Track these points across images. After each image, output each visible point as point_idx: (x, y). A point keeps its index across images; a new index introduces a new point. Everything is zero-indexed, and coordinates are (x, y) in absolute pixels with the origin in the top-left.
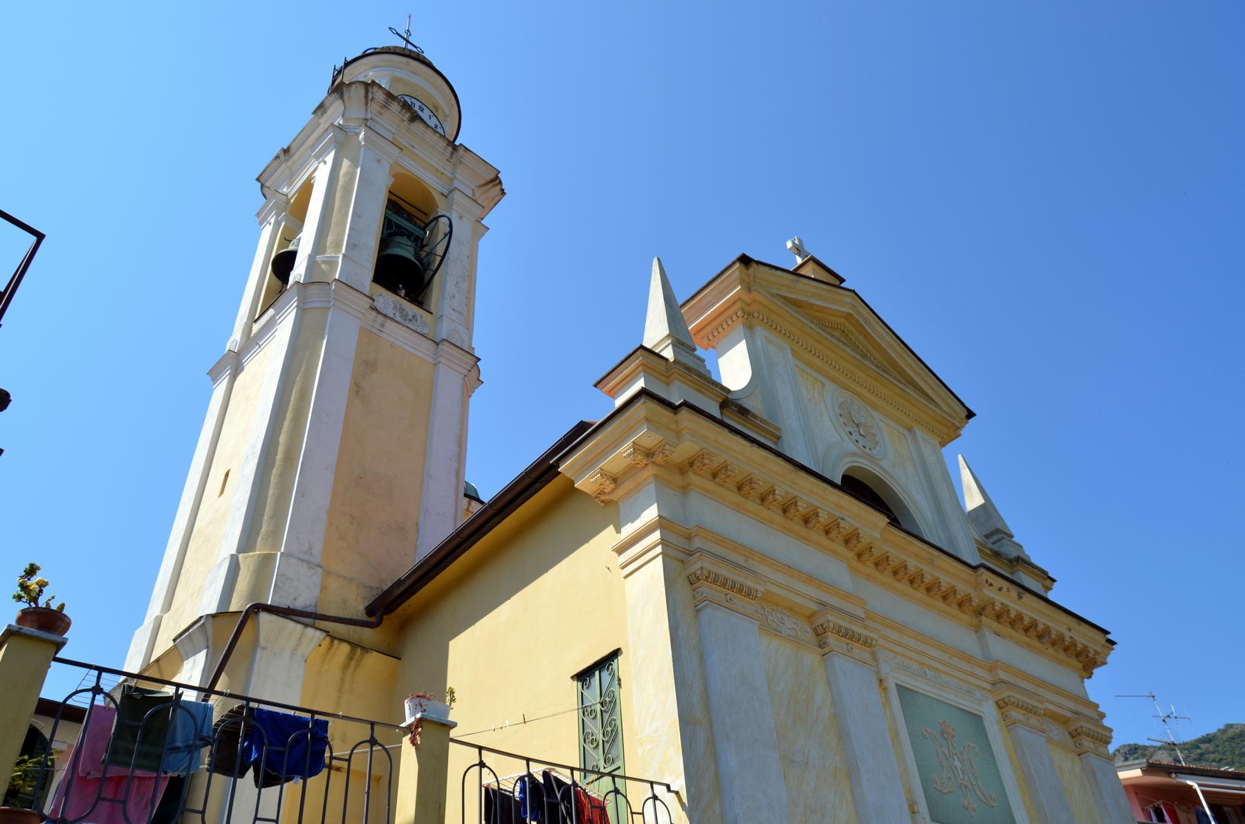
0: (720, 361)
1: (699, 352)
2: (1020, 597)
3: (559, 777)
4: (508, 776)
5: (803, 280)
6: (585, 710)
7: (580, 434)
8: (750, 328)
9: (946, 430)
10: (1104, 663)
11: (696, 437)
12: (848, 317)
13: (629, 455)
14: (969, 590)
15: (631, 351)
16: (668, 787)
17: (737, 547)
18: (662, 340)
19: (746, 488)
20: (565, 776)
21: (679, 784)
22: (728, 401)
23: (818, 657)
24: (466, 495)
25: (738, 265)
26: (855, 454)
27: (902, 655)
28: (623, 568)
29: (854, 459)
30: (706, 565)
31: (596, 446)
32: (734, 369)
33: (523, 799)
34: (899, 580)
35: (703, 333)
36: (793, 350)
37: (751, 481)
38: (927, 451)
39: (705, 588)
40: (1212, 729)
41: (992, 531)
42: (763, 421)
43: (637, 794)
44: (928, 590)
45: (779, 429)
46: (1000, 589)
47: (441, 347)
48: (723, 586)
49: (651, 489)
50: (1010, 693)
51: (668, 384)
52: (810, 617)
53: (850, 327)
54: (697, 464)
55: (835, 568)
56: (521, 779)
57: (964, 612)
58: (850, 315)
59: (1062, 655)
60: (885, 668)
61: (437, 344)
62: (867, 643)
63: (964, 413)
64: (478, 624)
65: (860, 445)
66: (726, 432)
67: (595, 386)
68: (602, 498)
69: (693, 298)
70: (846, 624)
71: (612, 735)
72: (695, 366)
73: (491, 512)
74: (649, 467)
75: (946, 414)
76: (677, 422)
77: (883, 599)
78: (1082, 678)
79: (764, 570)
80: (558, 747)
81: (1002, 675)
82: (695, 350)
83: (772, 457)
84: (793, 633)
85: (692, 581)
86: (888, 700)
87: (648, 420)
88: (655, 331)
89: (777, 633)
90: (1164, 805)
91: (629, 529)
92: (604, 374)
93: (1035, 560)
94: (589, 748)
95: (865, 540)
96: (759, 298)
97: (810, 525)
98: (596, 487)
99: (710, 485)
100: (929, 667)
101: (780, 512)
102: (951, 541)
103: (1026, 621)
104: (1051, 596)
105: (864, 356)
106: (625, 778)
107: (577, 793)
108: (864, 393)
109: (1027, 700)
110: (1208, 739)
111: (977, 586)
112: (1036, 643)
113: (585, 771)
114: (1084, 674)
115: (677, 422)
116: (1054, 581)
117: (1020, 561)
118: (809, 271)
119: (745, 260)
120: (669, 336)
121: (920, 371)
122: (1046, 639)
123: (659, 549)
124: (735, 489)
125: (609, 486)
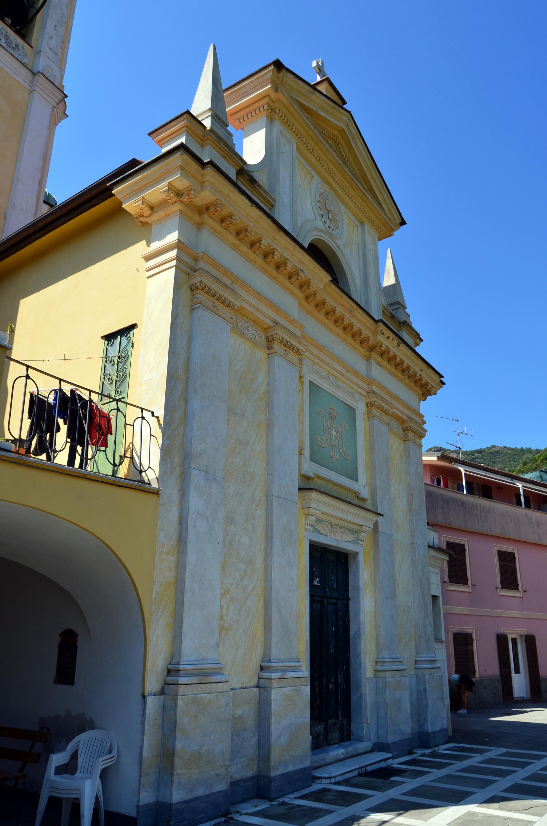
0: (244, 140)
1: (230, 128)
2: (398, 345)
3: (81, 395)
4: (46, 388)
5: (317, 94)
6: (107, 359)
7: (131, 168)
8: (271, 120)
9: (384, 229)
10: (435, 394)
11: (214, 190)
12: (342, 131)
13: (164, 191)
14: (369, 334)
15: (179, 113)
16: (153, 413)
17: (227, 272)
18: (205, 112)
19: (242, 235)
20: (85, 395)
21: (160, 412)
22: (243, 170)
23: (265, 355)
24: (45, 202)
25: (272, 67)
26: (321, 231)
27: (318, 364)
28: (147, 271)
29: (320, 234)
30: (204, 280)
31: (141, 179)
32: (253, 148)
33: (55, 404)
34: (328, 319)
35: (236, 116)
36: (297, 145)
37: (246, 230)
38: (369, 241)
39: (201, 296)
40: (484, 447)
41: (394, 300)
42: (265, 191)
43: (132, 414)
44: (345, 329)
45: (275, 200)
46: (388, 338)
47: (36, 77)
48: (213, 296)
49: (176, 220)
50: (376, 399)
51: (202, 146)
52: (266, 329)
53: (341, 140)
54: (212, 209)
55: (289, 301)
56: (55, 390)
57: (363, 347)
58: (343, 130)
59: (412, 385)
60: (305, 370)
61: (34, 74)
62: (298, 352)
63: (399, 221)
64: (43, 292)
65: (327, 225)
66: (236, 191)
67: (150, 135)
68: (141, 219)
69: (234, 85)
70: (287, 338)
71: (122, 377)
72: (225, 138)
73: (60, 213)
74: (178, 204)
75: (389, 219)
76: (203, 175)
77: (316, 329)
78: (420, 400)
79: (243, 293)
80: (86, 377)
81: (374, 388)
82: (227, 126)
83: (264, 217)
84: (253, 337)
85: (193, 289)
86: (302, 389)
87: (182, 168)
88: (201, 104)
89: (242, 335)
90: (443, 477)
91: (156, 245)
92: (157, 127)
93: (414, 326)
94: (106, 383)
95: (313, 288)
96: (283, 99)
97: (280, 270)
98: (138, 211)
99: (218, 227)
100: (333, 375)
101: (262, 257)
102: (367, 302)
103: (398, 360)
104: (417, 349)
105: (345, 163)
106: (127, 403)
107: (91, 407)
108: (339, 190)
109: (384, 405)
110: (480, 451)
111: (375, 333)
112: (400, 375)
113: (102, 395)
114: (421, 397)
115: (203, 175)
116: (422, 341)
117: (406, 324)
118: (322, 88)
119: (278, 65)
120: (210, 109)
121: (379, 184)
122: (399, 368)
123: (174, 263)
124: (235, 234)
125: (147, 212)
